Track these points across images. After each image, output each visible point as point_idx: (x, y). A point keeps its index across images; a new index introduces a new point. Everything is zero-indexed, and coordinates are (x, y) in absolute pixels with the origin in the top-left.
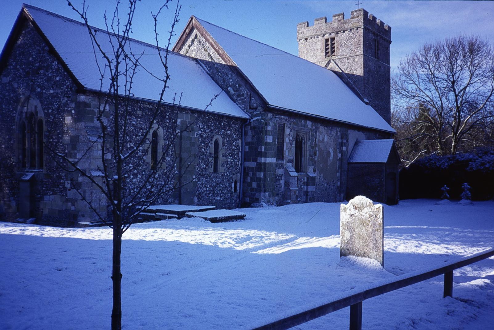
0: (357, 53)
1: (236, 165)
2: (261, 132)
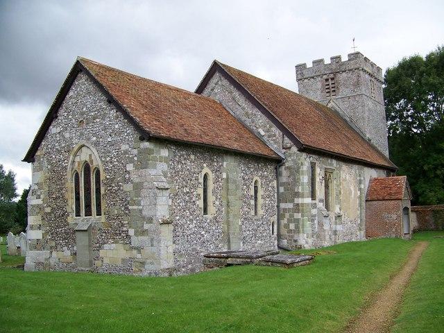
1: (273, 206)
2: (298, 171)
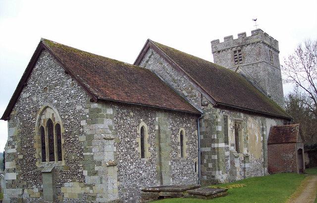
0: (260, 61)
